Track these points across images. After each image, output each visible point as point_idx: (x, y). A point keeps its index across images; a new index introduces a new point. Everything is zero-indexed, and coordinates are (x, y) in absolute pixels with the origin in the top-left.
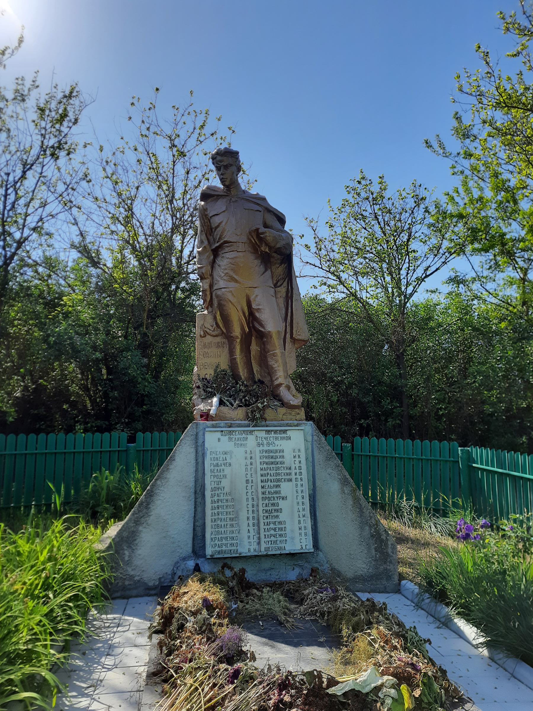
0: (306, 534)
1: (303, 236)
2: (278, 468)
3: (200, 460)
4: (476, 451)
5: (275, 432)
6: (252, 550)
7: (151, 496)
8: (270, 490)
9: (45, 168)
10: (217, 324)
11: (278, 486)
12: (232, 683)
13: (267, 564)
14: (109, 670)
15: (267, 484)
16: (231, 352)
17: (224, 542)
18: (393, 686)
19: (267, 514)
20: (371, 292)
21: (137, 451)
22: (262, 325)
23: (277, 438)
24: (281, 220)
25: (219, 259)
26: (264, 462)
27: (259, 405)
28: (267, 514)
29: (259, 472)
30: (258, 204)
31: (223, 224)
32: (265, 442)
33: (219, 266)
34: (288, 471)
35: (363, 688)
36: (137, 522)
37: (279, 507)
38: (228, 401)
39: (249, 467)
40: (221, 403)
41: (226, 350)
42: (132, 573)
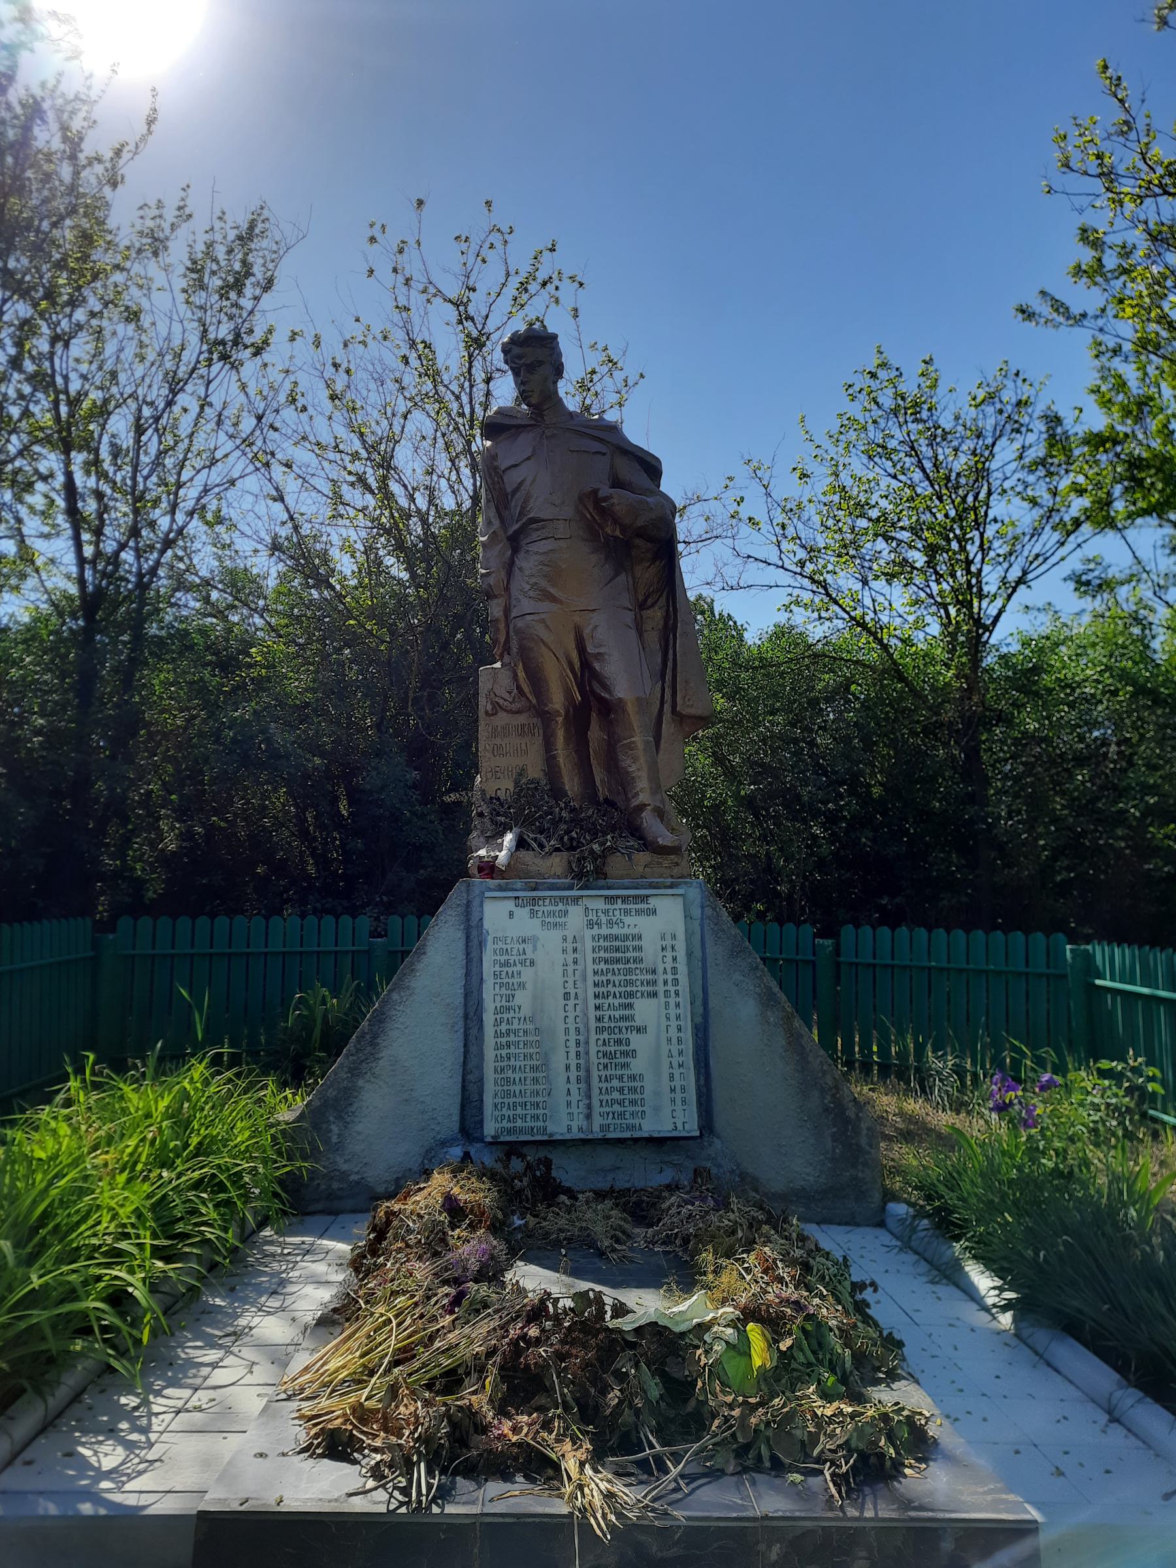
0: (684, 1102)
1: (742, 499)
2: (630, 971)
3: (474, 954)
4: (1099, 952)
5: (625, 899)
6: (575, 1129)
7: (381, 1022)
8: (612, 1013)
9: (212, 387)
10: (519, 687)
11: (630, 1006)
12: (452, 1312)
13: (607, 1158)
14: (269, 1313)
15: (606, 1002)
16: (548, 745)
17: (519, 1111)
18: (732, 1324)
19: (606, 1061)
20: (907, 614)
21: (390, 952)
22: (606, 687)
23: (627, 912)
24: (651, 468)
25: (522, 555)
26: (600, 960)
27: (596, 847)
28: (606, 1061)
29: (591, 978)
30: (601, 440)
31: (528, 482)
32: (604, 919)
33: (520, 569)
34: (650, 977)
35: (677, 1323)
36: (355, 1071)
37: (631, 1047)
38: (535, 840)
39: (570, 969)
40: (521, 844)
41: (539, 740)
42: (345, 1167)
